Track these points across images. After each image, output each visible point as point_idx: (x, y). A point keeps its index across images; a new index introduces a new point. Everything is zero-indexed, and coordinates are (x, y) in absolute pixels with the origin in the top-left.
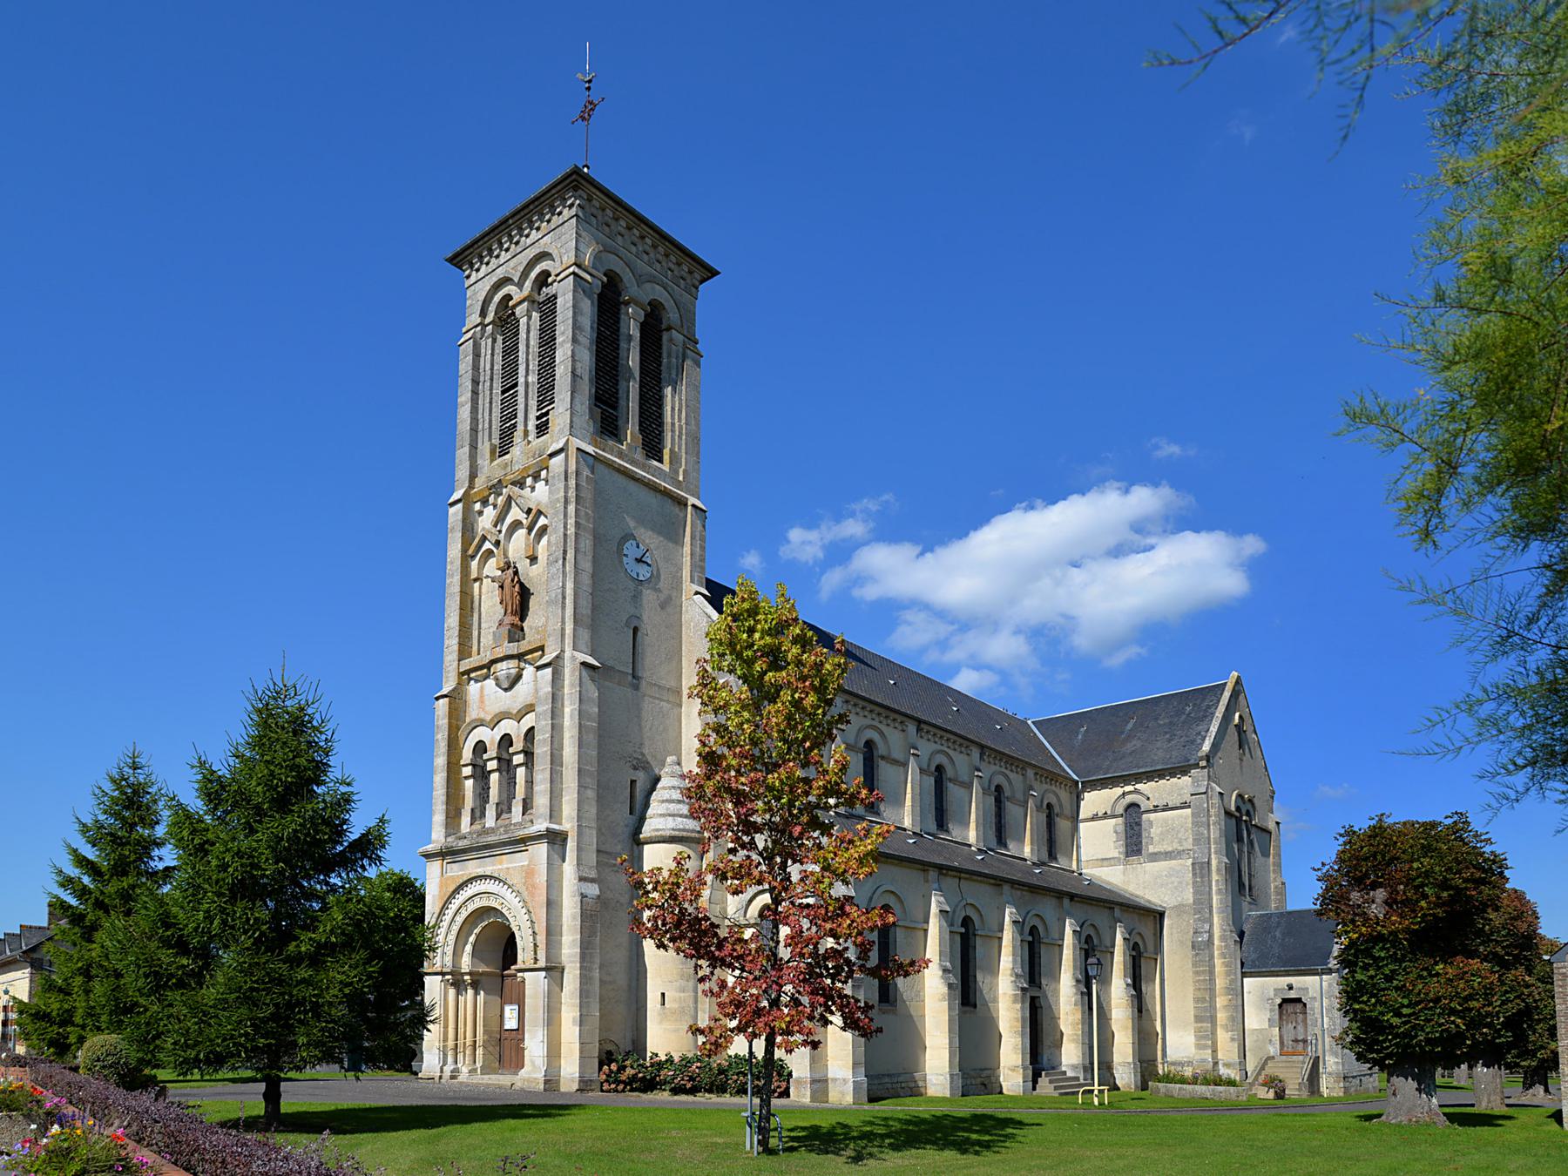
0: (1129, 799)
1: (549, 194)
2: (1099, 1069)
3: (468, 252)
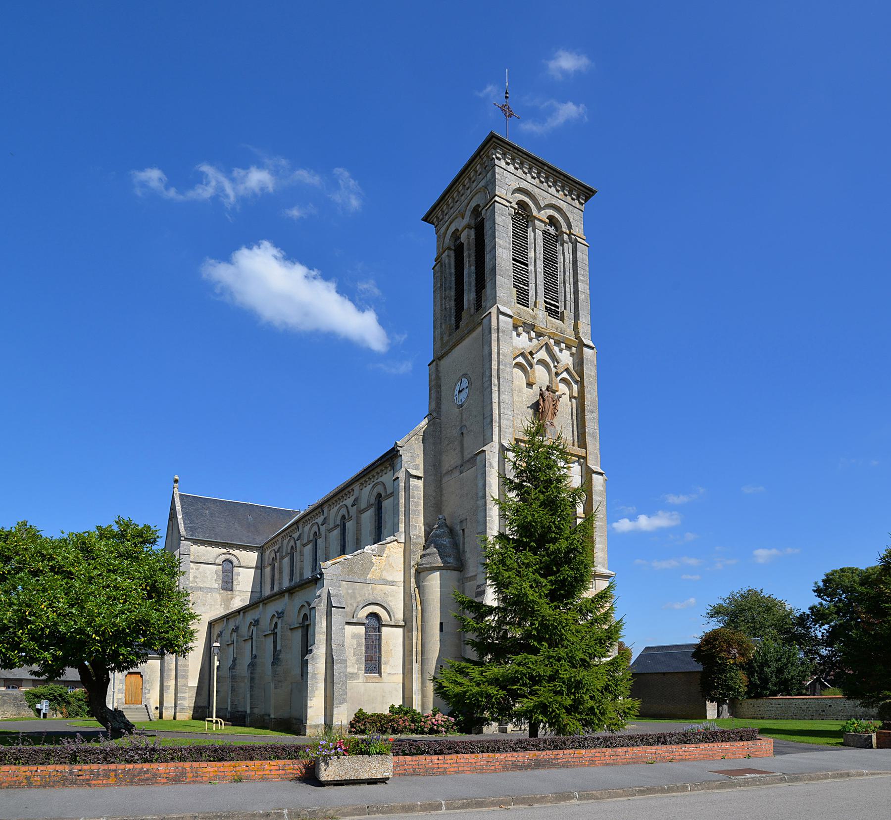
0: (228, 556)
1: (575, 185)
2: (216, 696)
3: (509, 147)
